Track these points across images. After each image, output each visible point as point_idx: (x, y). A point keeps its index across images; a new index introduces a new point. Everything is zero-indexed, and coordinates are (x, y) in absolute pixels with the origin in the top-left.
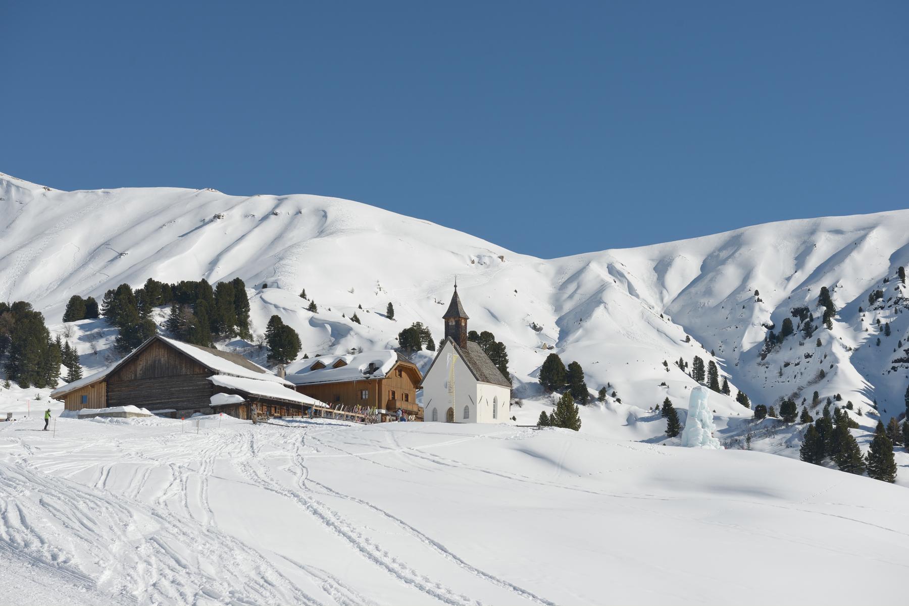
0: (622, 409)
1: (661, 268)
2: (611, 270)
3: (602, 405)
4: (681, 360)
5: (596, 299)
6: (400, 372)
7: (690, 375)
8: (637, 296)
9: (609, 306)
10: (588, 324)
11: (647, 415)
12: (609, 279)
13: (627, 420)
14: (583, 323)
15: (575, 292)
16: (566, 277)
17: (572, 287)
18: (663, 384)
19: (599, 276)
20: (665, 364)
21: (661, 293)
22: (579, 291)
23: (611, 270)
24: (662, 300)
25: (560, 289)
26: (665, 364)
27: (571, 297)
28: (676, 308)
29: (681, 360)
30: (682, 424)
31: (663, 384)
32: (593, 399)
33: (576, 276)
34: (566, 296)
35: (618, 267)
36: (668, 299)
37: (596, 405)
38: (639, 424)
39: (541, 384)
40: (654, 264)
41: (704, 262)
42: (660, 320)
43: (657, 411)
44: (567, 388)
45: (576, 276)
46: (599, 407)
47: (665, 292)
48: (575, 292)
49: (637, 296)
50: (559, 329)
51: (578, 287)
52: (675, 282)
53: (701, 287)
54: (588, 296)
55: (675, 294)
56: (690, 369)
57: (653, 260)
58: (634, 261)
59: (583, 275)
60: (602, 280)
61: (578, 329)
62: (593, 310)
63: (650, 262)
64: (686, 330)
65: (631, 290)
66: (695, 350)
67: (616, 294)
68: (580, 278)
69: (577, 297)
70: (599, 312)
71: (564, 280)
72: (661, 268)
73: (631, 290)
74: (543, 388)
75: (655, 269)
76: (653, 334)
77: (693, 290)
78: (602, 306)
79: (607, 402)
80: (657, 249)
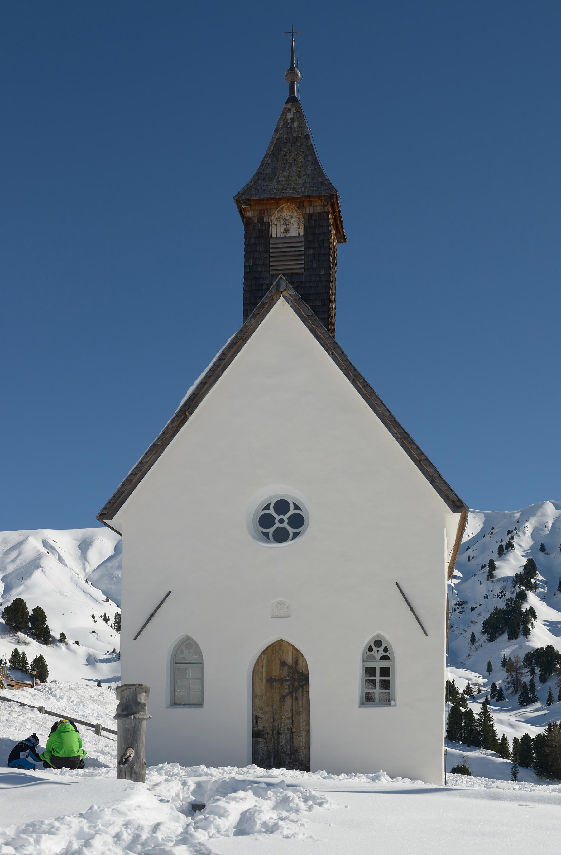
0: (82, 651)
1: (84, 546)
2: (45, 544)
3: (63, 646)
4: (105, 615)
5: (35, 564)
6: (522, 704)
7: (111, 627)
8: (66, 565)
9: (46, 570)
10: (28, 582)
11: (105, 657)
12: (44, 550)
13: (87, 660)
14: (23, 581)
15: (18, 556)
16: (9, 546)
17: (14, 554)
18: (94, 632)
19: (36, 547)
20: (93, 617)
21: (84, 565)
22: (20, 557)
23: (45, 544)
24: (85, 570)
25: (4, 555)
26: (93, 617)
27: (13, 561)
28: (96, 576)
29: (105, 615)
30: (11, 635)
31: (94, 632)
32: (54, 641)
33: (18, 546)
34: (10, 560)
35: (51, 542)
36: (89, 569)
37: (57, 646)
38: (98, 664)
39: (7, 624)
40: (78, 543)
41: (117, 545)
42: (85, 584)
43: (114, 655)
44: (31, 628)
45: (18, 546)
46: (60, 647)
47: (87, 564)
48: (18, 556)
49: (66, 565)
50: (4, 584)
51: (19, 554)
52: (95, 557)
53: (114, 563)
54: (27, 562)
55: (95, 566)
56: (112, 621)
57: (77, 540)
58: (64, 540)
59: (24, 545)
60: (39, 551)
61: (20, 585)
62: (32, 572)
63: (75, 541)
64: (104, 593)
65: (60, 559)
66: (112, 609)
67: (50, 561)
68: (21, 547)
69: (18, 561)
70: (37, 574)
71: (7, 548)
72: (84, 546)
73: (60, 559)
74: (8, 628)
75: (78, 547)
76: (81, 595)
77: (109, 564)
78: (40, 570)
79: (67, 644)
80: (80, 532)
